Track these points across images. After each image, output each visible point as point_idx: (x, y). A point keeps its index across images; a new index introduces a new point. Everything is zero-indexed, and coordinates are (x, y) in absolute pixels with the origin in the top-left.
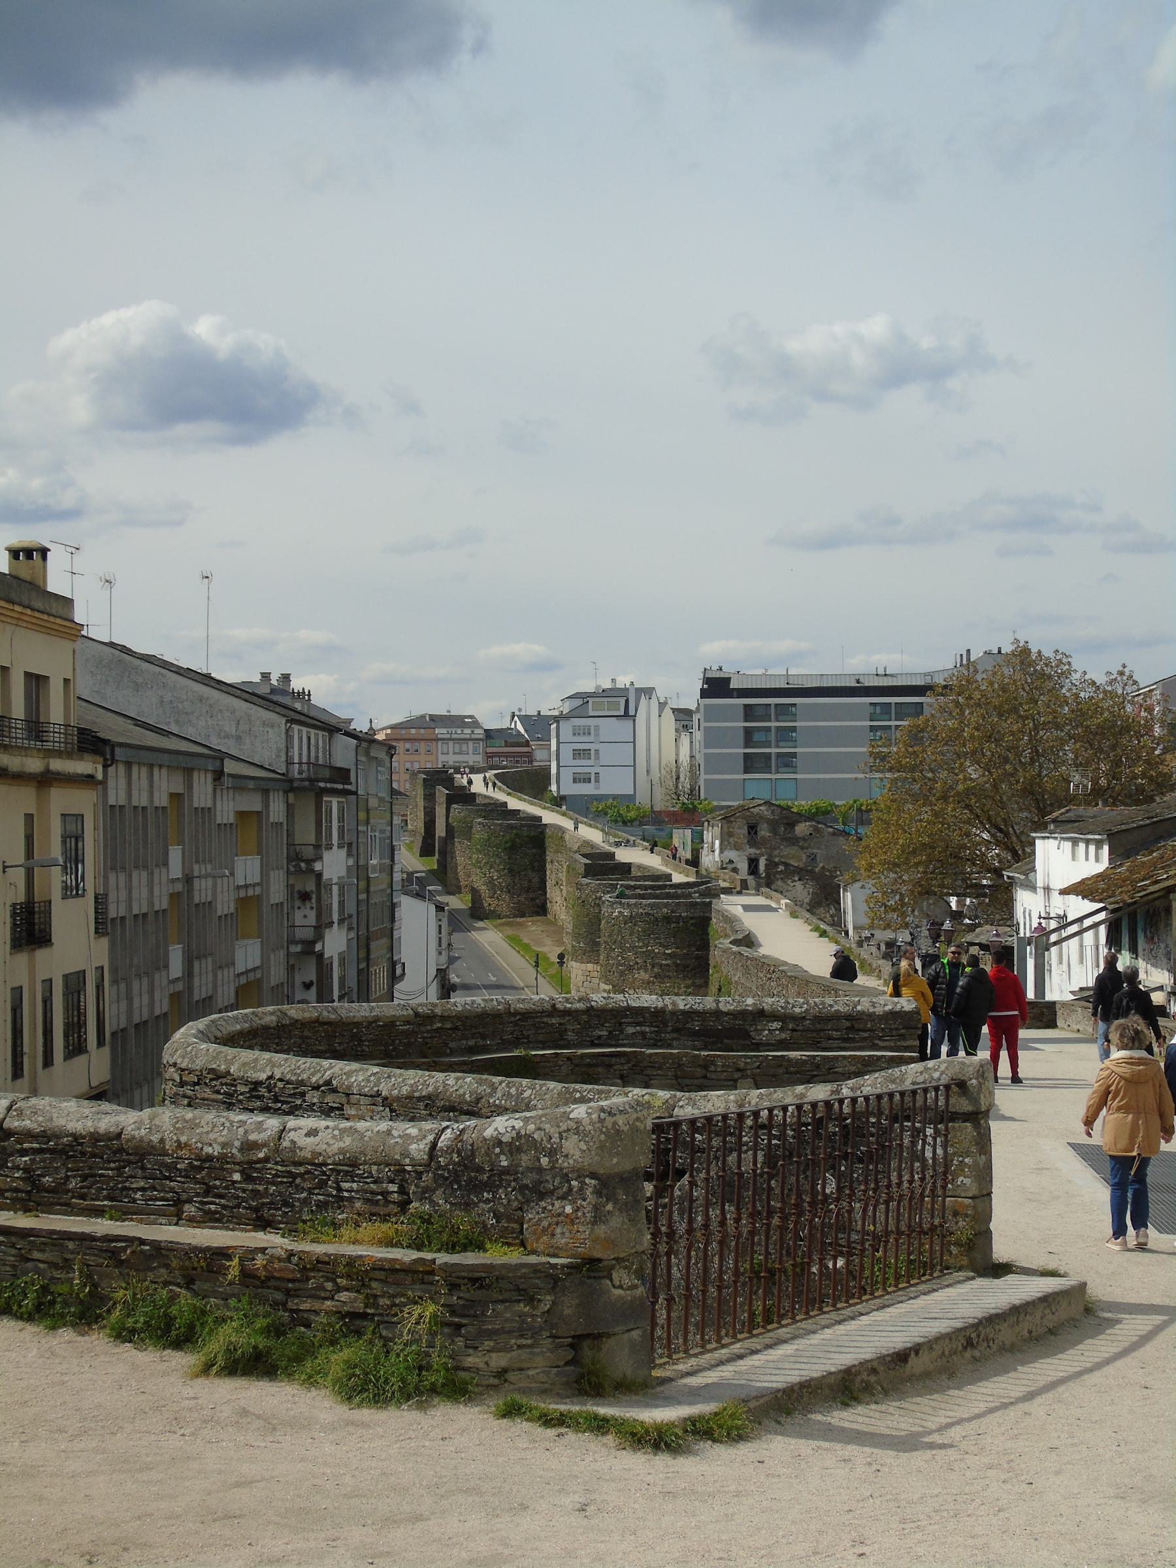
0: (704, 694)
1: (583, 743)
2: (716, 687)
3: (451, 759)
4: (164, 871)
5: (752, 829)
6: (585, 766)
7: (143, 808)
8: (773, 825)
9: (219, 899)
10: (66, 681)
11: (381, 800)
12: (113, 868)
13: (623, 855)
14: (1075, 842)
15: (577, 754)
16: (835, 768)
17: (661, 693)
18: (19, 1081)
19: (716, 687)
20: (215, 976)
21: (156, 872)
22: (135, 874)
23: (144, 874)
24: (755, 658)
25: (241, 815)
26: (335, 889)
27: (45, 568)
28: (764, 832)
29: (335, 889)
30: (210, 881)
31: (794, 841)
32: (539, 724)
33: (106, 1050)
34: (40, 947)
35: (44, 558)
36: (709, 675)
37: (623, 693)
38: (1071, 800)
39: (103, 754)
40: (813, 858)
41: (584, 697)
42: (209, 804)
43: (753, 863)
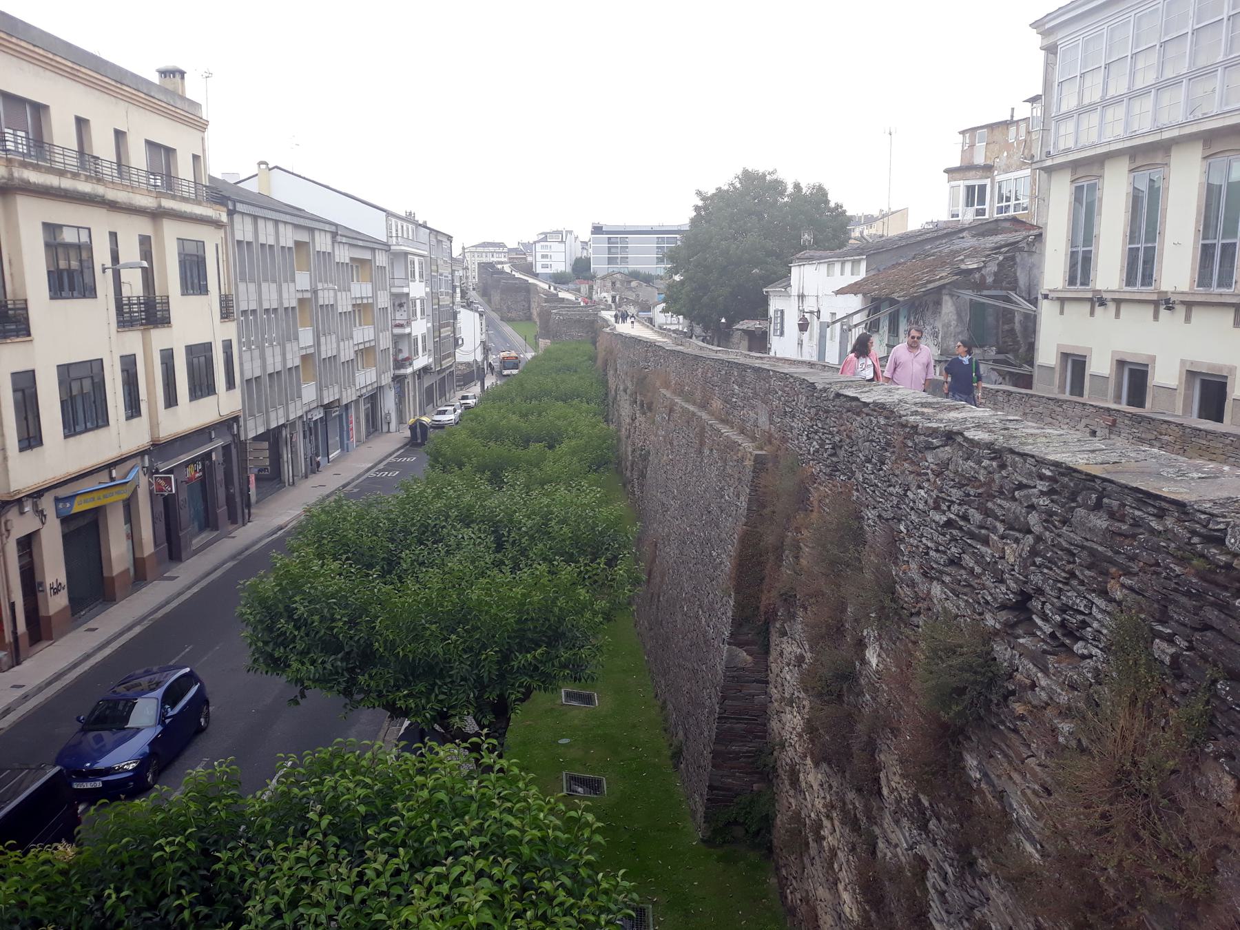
0: (593, 233)
1: (545, 252)
2: (597, 230)
3: (495, 259)
4: (291, 285)
5: (614, 284)
6: (545, 261)
7: (248, 243)
8: (622, 282)
9: (339, 302)
10: (196, 158)
11: (445, 262)
12: (243, 279)
13: (562, 295)
14: (830, 264)
15: (543, 256)
16: (645, 258)
17: (575, 233)
18: (135, 421)
19: (597, 230)
20: (338, 346)
21: (285, 286)
22: (264, 286)
23: (273, 286)
24: (610, 220)
25: (297, 243)
26: (418, 302)
27: (183, 84)
28: (618, 285)
29: (418, 302)
30: (332, 293)
31: (631, 289)
32: (529, 247)
33: (237, 392)
34: (156, 327)
35: (183, 78)
36: (55, 293)
37: (561, 232)
38: (804, 248)
39: (226, 206)
40: (638, 296)
41: (546, 234)
42: (329, 250)
43: (614, 298)
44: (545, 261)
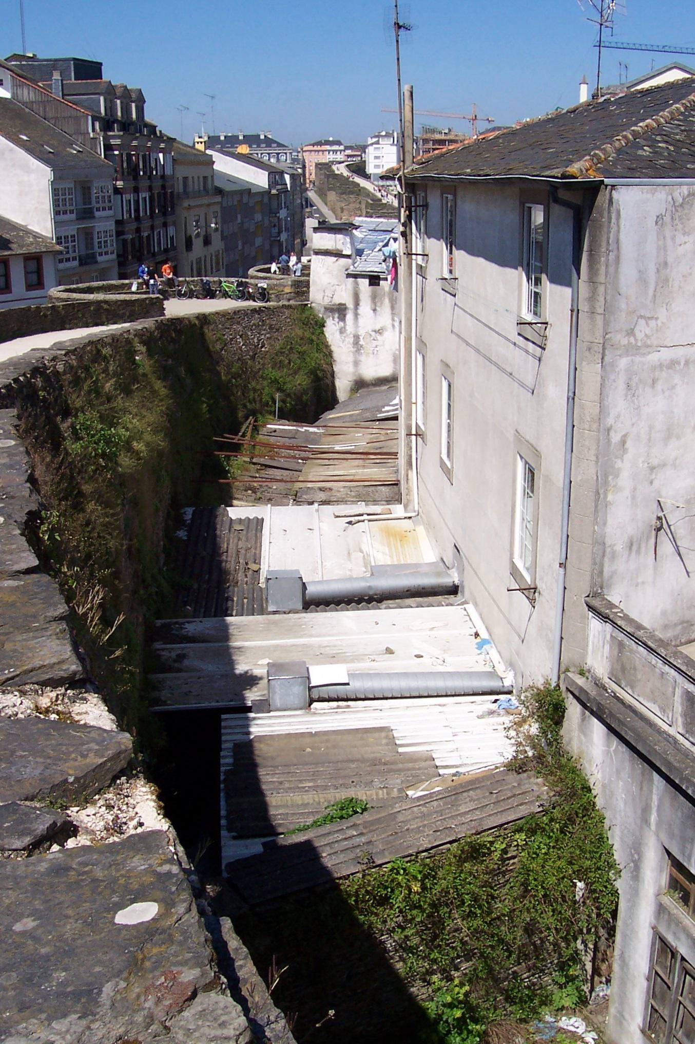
1: (378, 153)
15: (377, 158)
44: (377, 162)
